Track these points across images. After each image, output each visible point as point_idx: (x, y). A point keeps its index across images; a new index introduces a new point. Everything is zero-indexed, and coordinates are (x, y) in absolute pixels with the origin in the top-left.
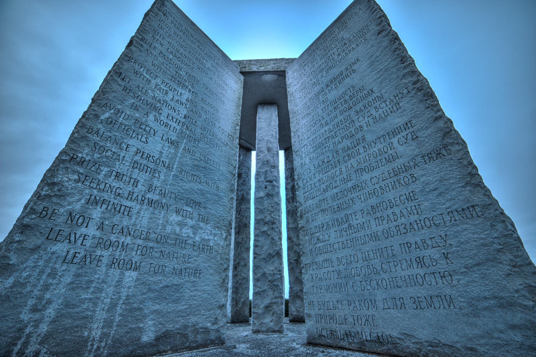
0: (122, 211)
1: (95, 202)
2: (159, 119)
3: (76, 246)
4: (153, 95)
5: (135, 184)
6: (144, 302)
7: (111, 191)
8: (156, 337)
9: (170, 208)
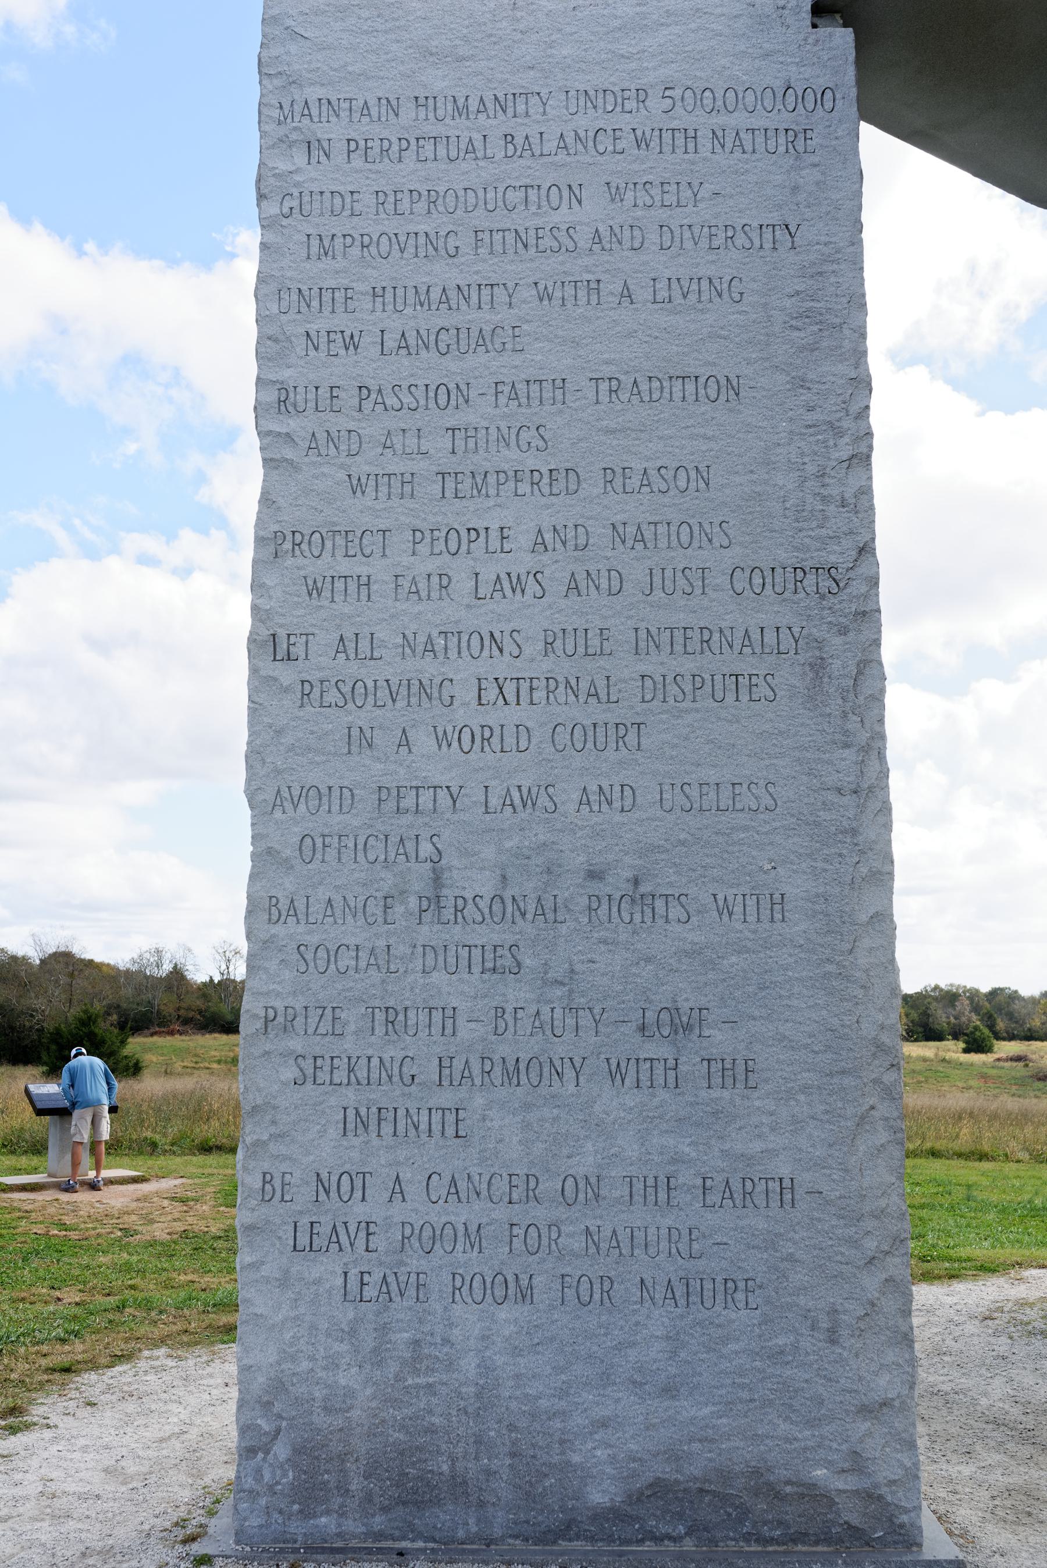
0: (436, 1128)
1: (360, 1125)
2: (449, 730)
3: (356, 1256)
4: (399, 640)
5: (449, 1023)
6: (568, 1394)
7: (390, 1077)
8: (630, 1496)
9: (586, 1070)
